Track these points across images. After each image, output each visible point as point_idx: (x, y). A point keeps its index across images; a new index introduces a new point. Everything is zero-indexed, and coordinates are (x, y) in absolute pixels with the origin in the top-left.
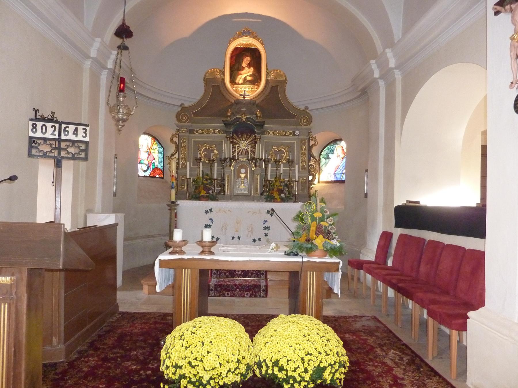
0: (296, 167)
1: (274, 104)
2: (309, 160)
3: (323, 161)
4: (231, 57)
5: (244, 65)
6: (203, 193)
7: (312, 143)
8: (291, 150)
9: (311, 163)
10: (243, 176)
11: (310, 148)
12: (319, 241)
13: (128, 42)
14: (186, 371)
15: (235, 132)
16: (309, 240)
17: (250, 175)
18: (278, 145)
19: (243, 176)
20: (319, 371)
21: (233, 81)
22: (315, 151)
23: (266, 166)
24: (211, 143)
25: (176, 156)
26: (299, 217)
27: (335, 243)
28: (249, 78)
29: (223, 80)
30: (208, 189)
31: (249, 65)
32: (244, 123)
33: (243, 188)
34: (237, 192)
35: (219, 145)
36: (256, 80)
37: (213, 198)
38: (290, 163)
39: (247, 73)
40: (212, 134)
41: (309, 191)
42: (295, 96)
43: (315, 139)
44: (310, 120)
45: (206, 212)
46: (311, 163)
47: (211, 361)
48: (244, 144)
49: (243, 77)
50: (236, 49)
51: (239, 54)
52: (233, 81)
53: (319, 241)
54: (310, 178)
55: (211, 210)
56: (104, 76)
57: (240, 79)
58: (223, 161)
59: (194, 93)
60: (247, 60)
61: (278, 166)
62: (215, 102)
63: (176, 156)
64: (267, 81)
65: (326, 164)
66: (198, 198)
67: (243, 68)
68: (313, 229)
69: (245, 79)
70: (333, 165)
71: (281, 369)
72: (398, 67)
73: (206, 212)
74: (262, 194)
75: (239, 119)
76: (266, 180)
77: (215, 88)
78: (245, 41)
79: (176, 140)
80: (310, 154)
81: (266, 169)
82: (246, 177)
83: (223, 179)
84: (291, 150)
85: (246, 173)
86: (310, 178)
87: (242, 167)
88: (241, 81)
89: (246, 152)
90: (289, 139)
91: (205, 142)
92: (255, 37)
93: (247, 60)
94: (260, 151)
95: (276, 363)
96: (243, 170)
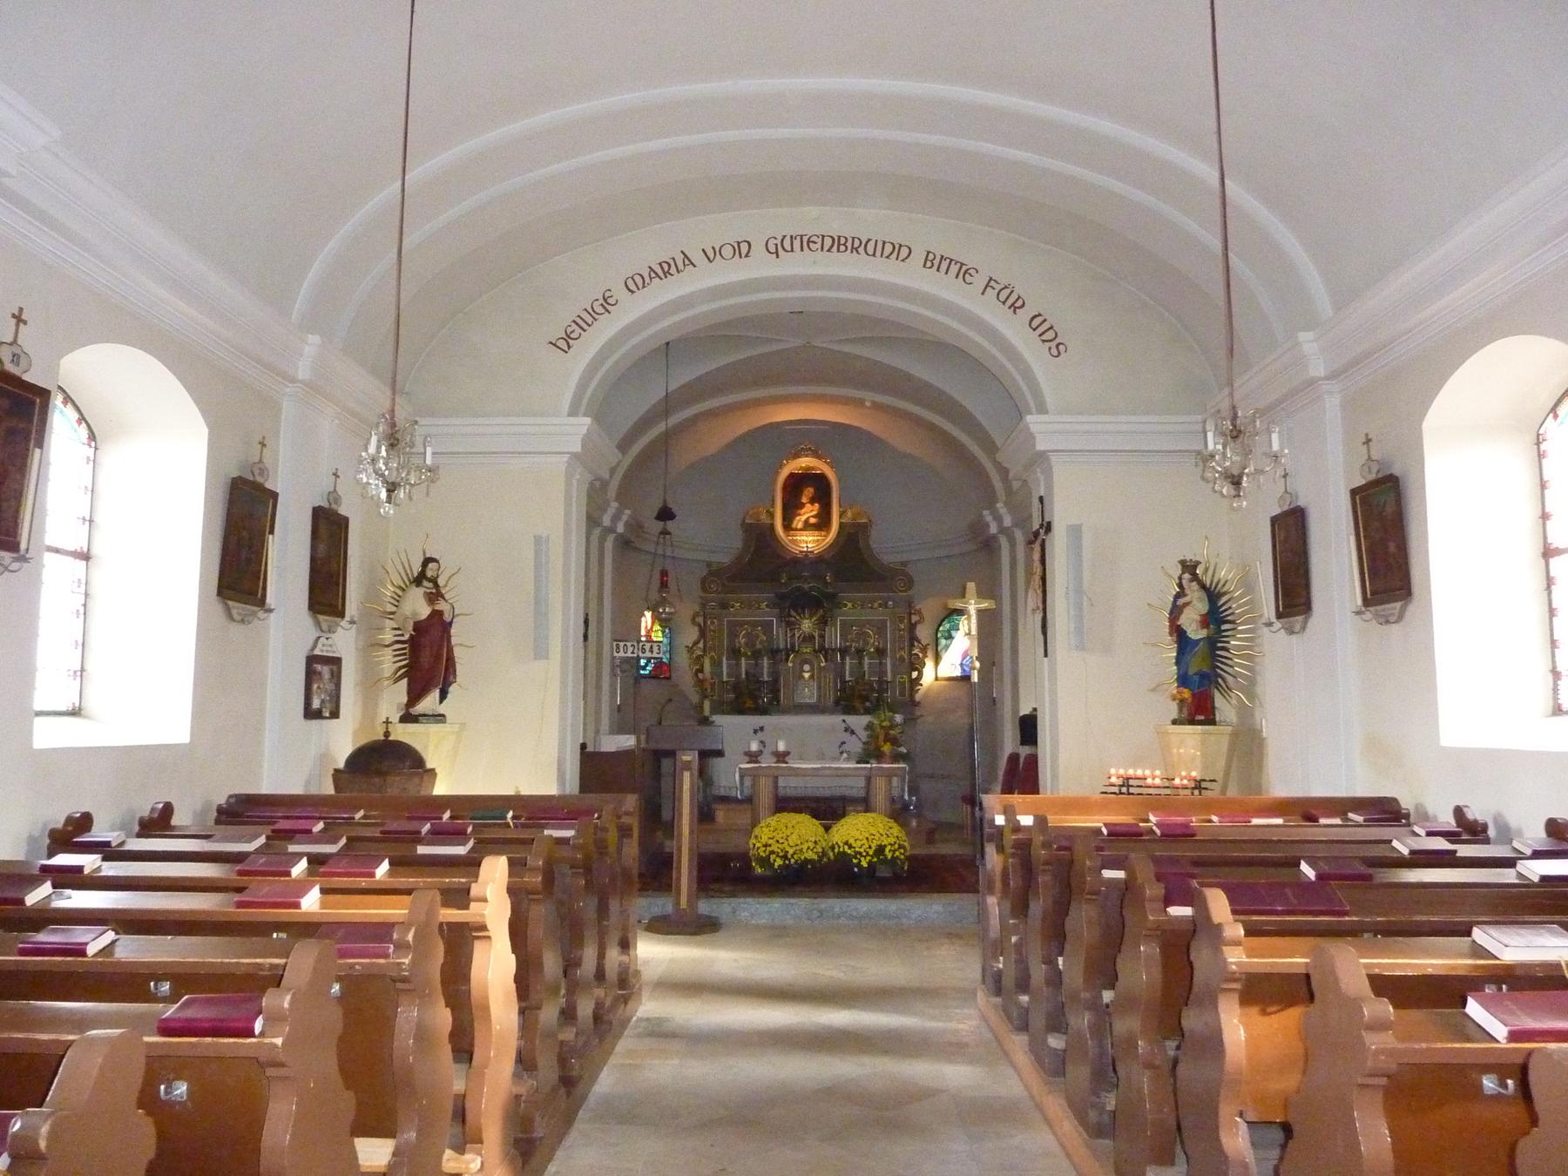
0: (889, 661)
1: (852, 560)
2: (912, 646)
3: (943, 642)
4: (785, 488)
5: (804, 500)
6: (749, 704)
7: (914, 618)
8: (881, 629)
9: (916, 651)
10: (807, 675)
11: (912, 627)
12: (887, 748)
13: (670, 525)
14: (775, 848)
15: (794, 606)
16: (878, 748)
17: (817, 675)
18: (862, 624)
19: (807, 675)
20: (880, 849)
21: (788, 527)
22: (923, 633)
23: (843, 658)
24: (754, 625)
25: (701, 645)
26: (869, 727)
27: (903, 750)
28: (813, 520)
29: (772, 527)
30: (753, 697)
31: (812, 501)
32: (807, 590)
33: (808, 694)
34: (799, 700)
35: (767, 627)
36: (822, 523)
37: (763, 711)
38: (881, 652)
39: (809, 512)
40: (756, 612)
41: (912, 696)
42: (886, 545)
43: (919, 612)
44: (910, 583)
45: (755, 732)
46: (916, 651)
47: (793, 839)
48: (807, 625)
49: (804, 518)
50: (792, 475)
51: (796, 484)
52: (788, 527)
53: (887, 748)
54: (915, 674)
55: (762, 729)
56: (611, 538)
57: (798, 522)
58: (774, 653)
59: (727, 546)
60: (809, 492)
61: (861, 659)
62: (761, 560)
63: (701, 645)
64: (841, 525)
65: (947, 647)
66: (741, 711)
67: (802, 506)
68: (882, 737)
69: (806, 521)
70: (955, 656)
71: (850, 847)
72: (1016, 525)
73: (755, 732)
74: (837, 703)
75: (799, 589)
76: (844, 682)
77: (760, 541)
78: (805, 462)
79: (700, 620)
80: (913, 639)
81: (843, 663)
82: (812, 677)
83: (776, 681)
84: (881, 629)
85: (812, 670)
86: (915, 674)
87: (806, 662)
88: (800, 526)
89: (812, 638)
90: (879, 614)
91: (748, 623)
92: (818, 457)
93: (809, 492)
94: (834, 637)
95: (846, 843)
96: (807, 667)
